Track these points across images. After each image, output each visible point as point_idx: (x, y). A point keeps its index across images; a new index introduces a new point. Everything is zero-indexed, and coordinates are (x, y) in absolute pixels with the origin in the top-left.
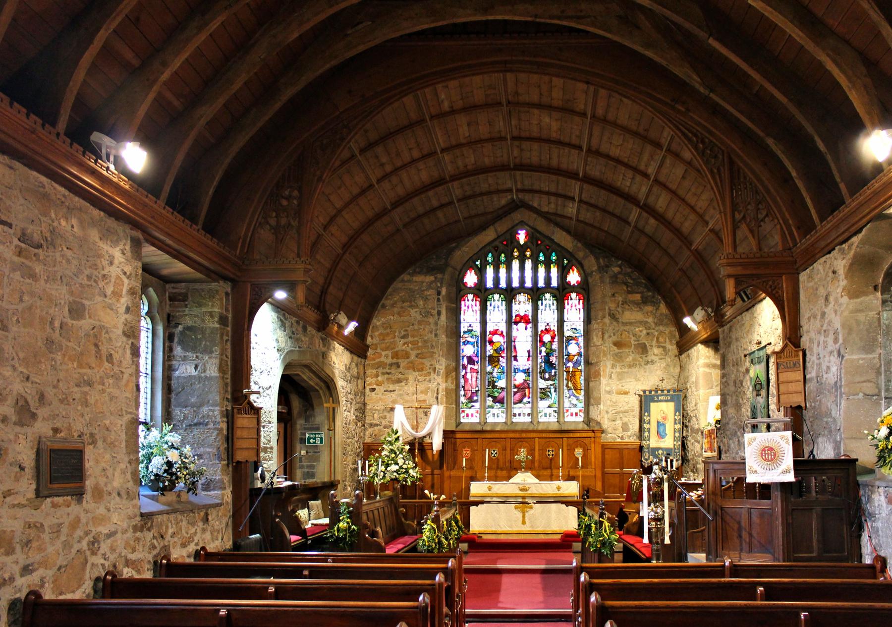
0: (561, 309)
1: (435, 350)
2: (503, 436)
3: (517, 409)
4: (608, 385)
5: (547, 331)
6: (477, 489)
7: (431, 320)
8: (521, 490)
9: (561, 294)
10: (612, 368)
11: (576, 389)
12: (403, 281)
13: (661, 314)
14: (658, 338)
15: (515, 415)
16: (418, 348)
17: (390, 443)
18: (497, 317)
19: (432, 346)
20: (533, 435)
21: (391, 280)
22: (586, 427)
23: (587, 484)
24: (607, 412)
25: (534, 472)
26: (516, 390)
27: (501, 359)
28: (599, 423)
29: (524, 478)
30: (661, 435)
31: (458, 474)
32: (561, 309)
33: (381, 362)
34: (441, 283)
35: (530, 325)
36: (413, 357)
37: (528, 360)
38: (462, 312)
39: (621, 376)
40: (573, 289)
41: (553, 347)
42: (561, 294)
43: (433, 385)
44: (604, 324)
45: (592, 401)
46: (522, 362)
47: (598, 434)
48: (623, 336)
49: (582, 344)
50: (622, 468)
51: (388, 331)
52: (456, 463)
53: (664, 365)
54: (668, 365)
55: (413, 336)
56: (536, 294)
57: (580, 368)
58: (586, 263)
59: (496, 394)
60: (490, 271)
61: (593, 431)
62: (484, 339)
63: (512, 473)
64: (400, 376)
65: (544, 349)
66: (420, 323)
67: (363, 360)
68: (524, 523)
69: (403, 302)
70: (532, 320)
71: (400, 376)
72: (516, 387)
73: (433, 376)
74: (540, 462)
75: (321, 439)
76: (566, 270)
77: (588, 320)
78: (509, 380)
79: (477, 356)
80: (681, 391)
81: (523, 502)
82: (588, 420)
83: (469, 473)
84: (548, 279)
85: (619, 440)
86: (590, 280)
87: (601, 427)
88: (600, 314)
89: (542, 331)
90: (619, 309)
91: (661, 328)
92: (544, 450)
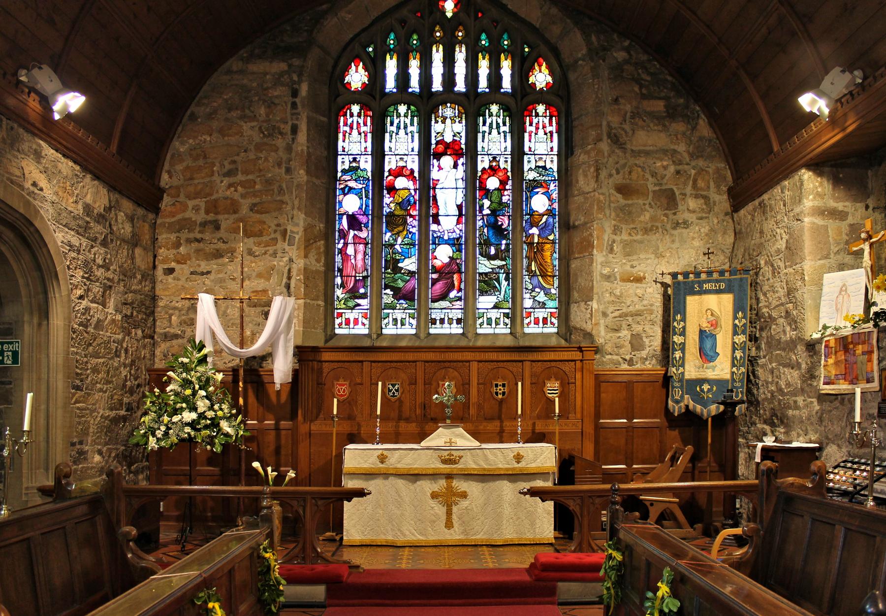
0: (518, 134)
1: (286, 198)
2: (410, 357)
4: (605, 264)
5: (493, 170)
6: (356, 456)
7: (280, 142)
8: (445, 462)
9: (519, 106)
10: (615, 232)
11: (544, 276)
12: (229, 72)
13: (701, 139)
14: (695, 181)
15: (434, 322)
16: (255, 195)
17: (186, 368)
18: (402, 146)
19: (281, 190)
20: (468, 356)
21: (209, 67)
22: (563, 343)
24: (605, 314)
25: (470, 426)
26: (435, 276)
27: (409, 220)
28: (589, 336)
29: (450, 438)
30: (707, 354)
31: (325, 429)
32: (518, 134)
33: (185, 219)
34: (300, 75)
35: (461, 161)
36: (244, 210)
37: (458, 222)
39: (629, 250)
40: (541, 96)
41: (505, 199)
42: (519, 106)
43: (281, 263)
44: (600, 152)
45: (575, 295)
46: (448, 224)
47: (588, 355)
48: (634, 176)
49: (555, 195)
50: (630, 419)
51: (201, 162)
52: (320, 408)
53: (705, 230)
54: (712, 230)
55: (246, 172)
56: (473, 106)
57: (551, 237)
58: (565, 48)
59: (400, 284)
60: (391, 66)
61: (580, 349)
62: (379, 184)
63: (427, 428)
64: (221, 245)
65: (487, 203)
66: (259, 147)
67: (151, 216)
68: (449, 524)
69: (230, 110)
70: (466, 152)
71: (221, 245)
72: (435, 270)
73: (280, 245)
74: (480, 407)
75: (15, 354)
76: (527, 65)
77: (566, 151)
78: (424, 257)
79: (365, 214)
80: (747, 271)
81: (450, 475)
82: (566, 328)
83: (346, 427)
84: (495, 78)
85: (625, 366)
86: (572, 76)
87: (593, 341)
88: (593, 133)
89: (484, 169)
90: (627, 127)
91: (701, 163)
92: (484, 388)
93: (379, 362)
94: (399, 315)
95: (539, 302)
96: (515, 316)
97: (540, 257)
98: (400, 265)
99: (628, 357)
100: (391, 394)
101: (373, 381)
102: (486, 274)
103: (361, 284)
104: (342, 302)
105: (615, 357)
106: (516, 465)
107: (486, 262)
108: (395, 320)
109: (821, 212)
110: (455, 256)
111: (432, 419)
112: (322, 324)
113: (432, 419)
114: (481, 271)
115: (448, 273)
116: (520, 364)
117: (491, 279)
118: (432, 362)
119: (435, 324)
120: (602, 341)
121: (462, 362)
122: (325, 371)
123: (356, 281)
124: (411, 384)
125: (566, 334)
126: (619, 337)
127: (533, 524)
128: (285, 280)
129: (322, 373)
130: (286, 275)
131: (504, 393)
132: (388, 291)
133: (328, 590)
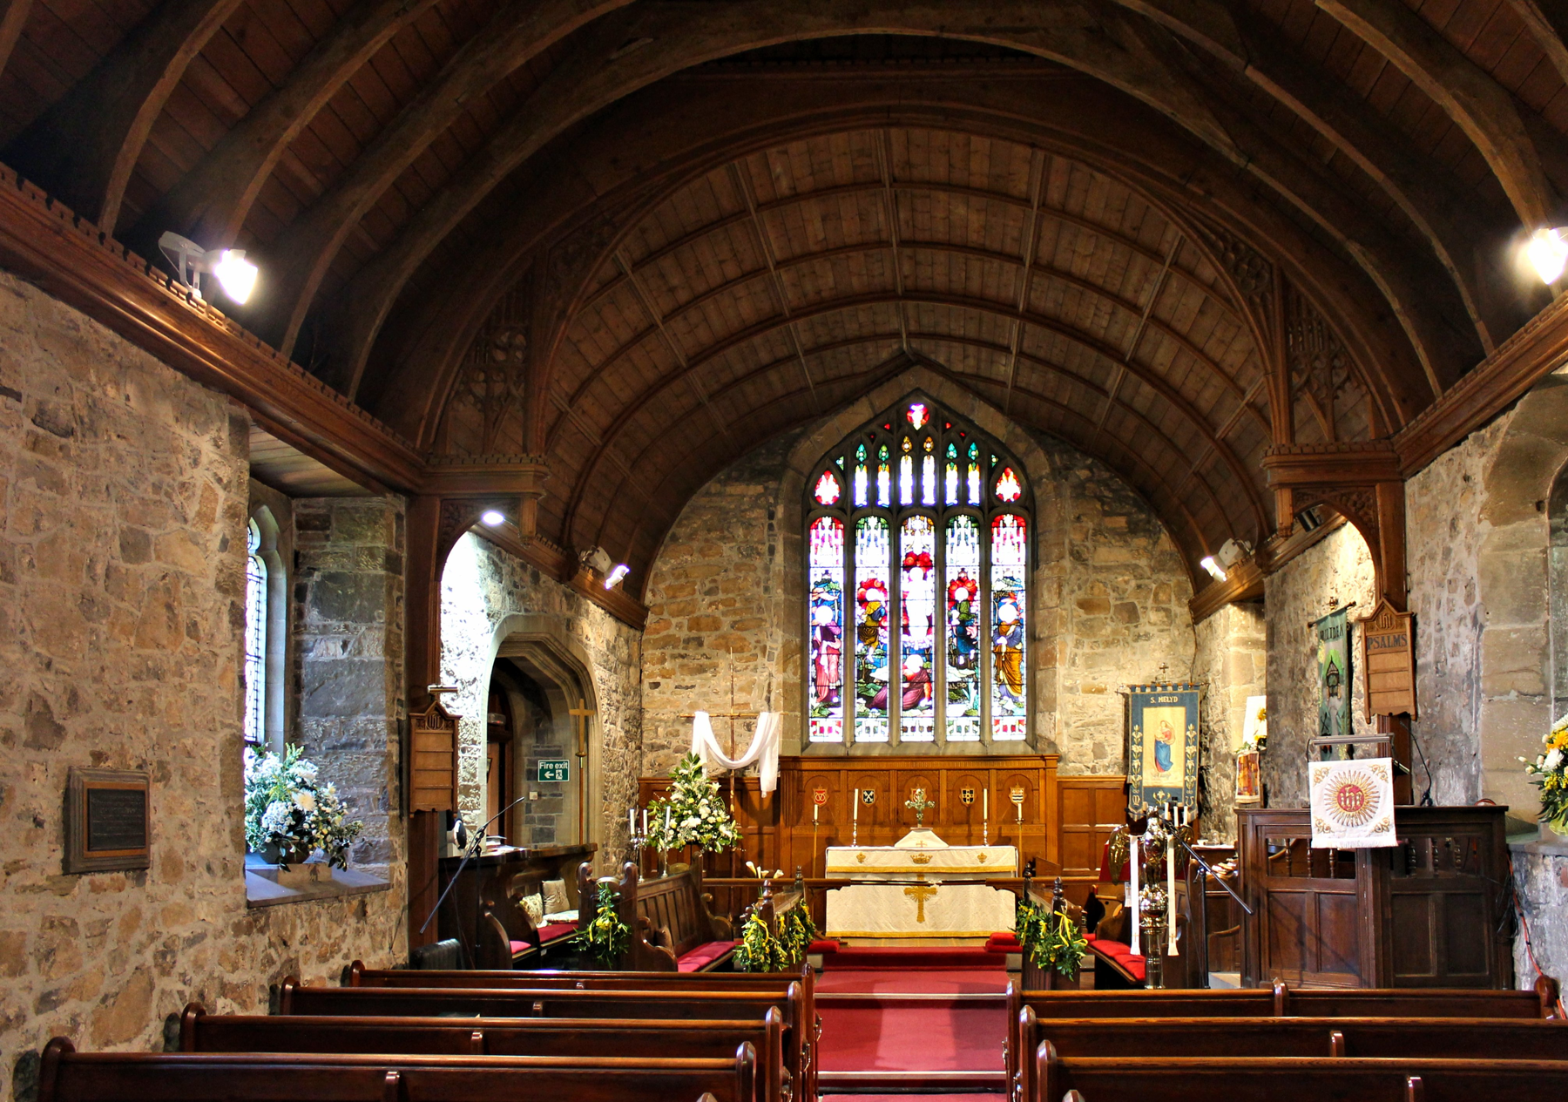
0: (986, 543)
1: (765, 616)
2: (884, 766)
3: (909, 718)
4: (1069, 676)
5: (962, 582)
6: (838, 859)
7: (758, 563)
8: (916, 861)
9: (987, 516)
11: (1012, 684)
12: (708, 494)
13: (1162, 553)
14: (1156, 595)
15: (905, 730)
16: (735, 612)
17: (687, 779)
18: (873, 556)
19: (760, 609)
20: (937, 765)
22: (1030, 751)
23: (1032, 850)
24: (1067, 724)
26: (906, 685)
27: (881, 631)
28: (1052, 744)
29: (922, 841)
30: (1161, 765)
31: (805, 832)
32: (986, 543)
34: (776, 498)
35: (931, 572)
36: (725, 628)
37: (929, 632)
39: (1091, 661)
40: (1008, 507)
41: (973, 610)
42: (987, 516)
43: (761, 677)
44: (1062, 569)
45: (1041, 705)
46: (918, 636)
47: (1051, 763)
48: (1096, 591)
49: (1023, 605)
50: (1093, 823)
51: (683, 581)
52: (801, 814)
53: (1166, 641)
54: (1173, 642)
55: (726, 591)
56: (941, 517)
57: (1019, 647)
58: (1030, 462)
59: (873, 693)
61: (1043, 758)
62: (851, 595)
63: (900, 832)
64: (704, 661)
65: (955, 613)
66: (738, 567)
67: (638, 634)
68: (921, 918)
69: (709, 531)
70: (935, 563)
72: (906, 679)
73: (761, 660)
74: (949, 812)
75: (565, 772)
76: (995, 476)
77: (1033, 563)
78: (894, 668)
79: (838, 625)
80: (1197, 687)
81: (919, 882)
82: (1033, 738)
83: (825, 832)
84: (963, 491)
85: (1088, 773)
88: (1056, 551)
89: (953, 582)
90: (1089, 544)
91: (1162, 576)
92: (957, 792)
94: (870, 722)
96: (983, 724)
109: (1245, 642)
122: (805, 780)
127: (996, 918)
133: (825, 960)
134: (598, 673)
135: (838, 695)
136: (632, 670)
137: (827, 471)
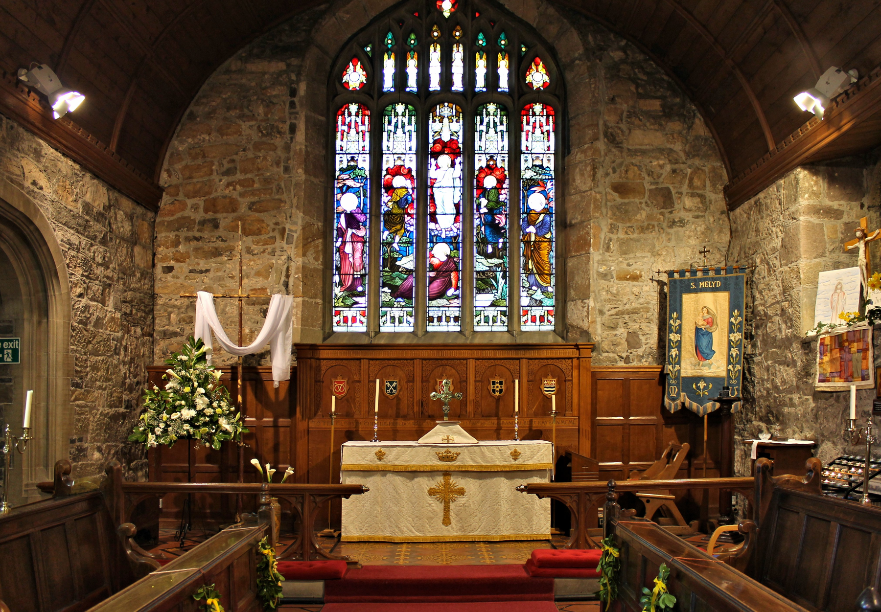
0: (515, 133)
1: (285, 197)
2: (408, 354)
4: (602, 262)
5: (490, 169)
6: (354, 453)
7: (278, 141)
8: (442, 459)
9: (516, 105)
11: (541, 274)
12: (228, 71)
13: (697, 138)
14: (691, 180)
15: (431, 320)
16: (253, 194)
17: (185, 366)
18: (400, 145)
19: (279, 188)
20: (465, 354)
22: (560, 341)
23: (564, 444)
24: (601, 312)
25: (467, 423)
26: (432, 274)
27: (407, 218)
28: (585, 333)
29: (447, 435)
30: (703, 352)
31: (323, 426)
32: (515, 133)
33: (184, 218)
34: (298, 74)
35: (459, 160)
36: (243, 209)
37: (456, 221)
38: (339, 135)
39: (626, 248)
40: (538, 96)
41: (502, 198)
42: (516, 105)
43: (279, 261)
44: (596, 151)
45: (572, 293)
46: (446, 223)
47: (585, 353)
48: (631, 174)
49: (552, 194)
50: (626, 416)
51: (200, 161)
52: (319, 405)
53: (701, 228)
54: (708, 228)
56: (470, 105)
57: (548, 236)
59: (398, 282)
61: (577, 347)
62: (377, 183)
63: (425, 425)
64: (220, 244)
65: (484, 201)
66: (257, 146)
67: (150, 215)
68: (446, 521)
69: (229, 109)
70: (463, 151)
71: (220, 244)
72: (433, 268)
73: (279, 243)
74: (477, 404)
75: (15, 352)
77: (563, 150)
78: (422, 256)
80: (742, 269)
81: (447, 472)
82: (563, 326)
83: (344, 425)
84: (492, 78)
85: (621, 364)
87: (589, 339)
88: (590, 133)
89: (481, 168)
90: (623, 126)
91: (697, 162)
92: (481, 385)
93: (377, 359)
94: (396, 312)
95: (536, 300)
96: (512, 314)
97: (537, 255)
98: (398, 263)
99: (624, 355)
100: (389, 391)
101: (371, 379)
102: (483, 272)
103: (359, 282)
104: (341, 300)
105: (611, 355)
106: (513, 462)
107: (484, 261)
108: (393, 318)
110: (452, 255)
111: (429, 416)
112: (320, 322)
113: (429, 416)
114: (478, 269)
115: (446, 271)
116: (358, 362)
117: (488, 277)
118: (430, 359)
119: (433, 322)
120: (598, 338)
121: (460, 359)
122: (324, 368)
123: (354, 279)
124: (408, 381)
125: (563, 331)
126: (616, 335)
127: (530, 520)
128: (283, 278)
129: (320, 370)
130: (284, 273)
131: (501, 391)
132: (386, 289)
133: (326, 587)
134: (59, 236)
135: (362, 285)
136: (137, 250)
137: (355, 58)
